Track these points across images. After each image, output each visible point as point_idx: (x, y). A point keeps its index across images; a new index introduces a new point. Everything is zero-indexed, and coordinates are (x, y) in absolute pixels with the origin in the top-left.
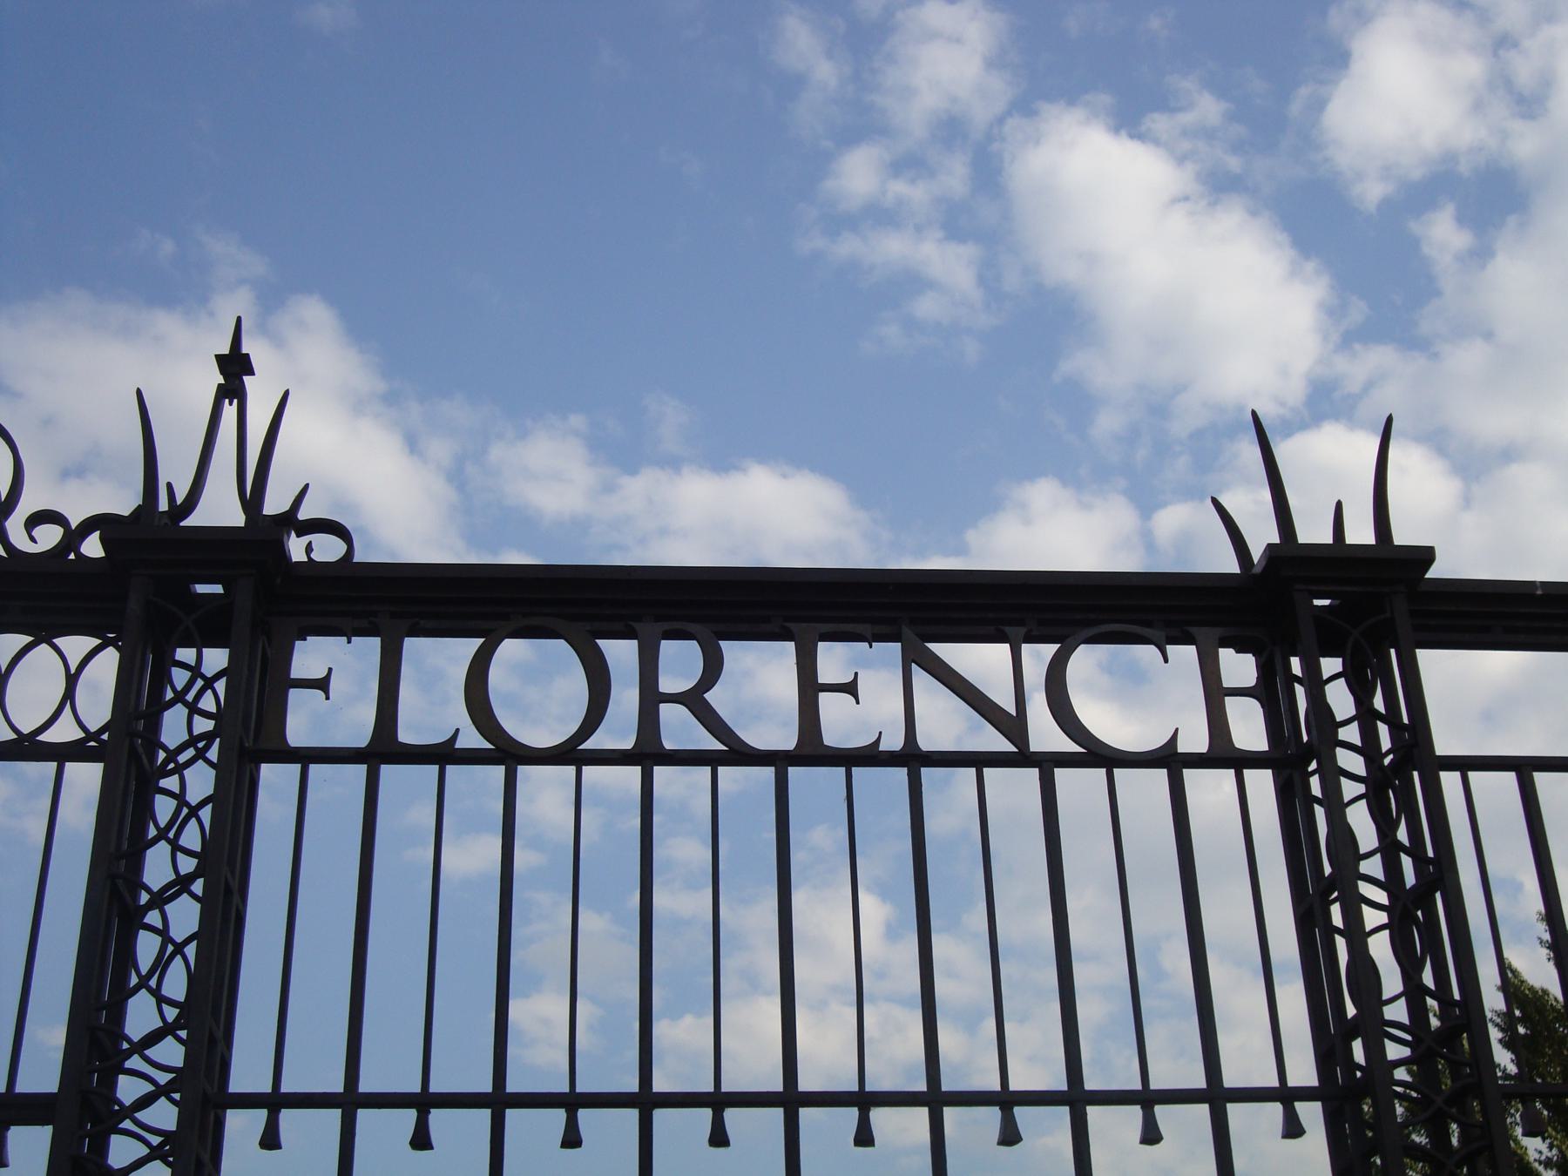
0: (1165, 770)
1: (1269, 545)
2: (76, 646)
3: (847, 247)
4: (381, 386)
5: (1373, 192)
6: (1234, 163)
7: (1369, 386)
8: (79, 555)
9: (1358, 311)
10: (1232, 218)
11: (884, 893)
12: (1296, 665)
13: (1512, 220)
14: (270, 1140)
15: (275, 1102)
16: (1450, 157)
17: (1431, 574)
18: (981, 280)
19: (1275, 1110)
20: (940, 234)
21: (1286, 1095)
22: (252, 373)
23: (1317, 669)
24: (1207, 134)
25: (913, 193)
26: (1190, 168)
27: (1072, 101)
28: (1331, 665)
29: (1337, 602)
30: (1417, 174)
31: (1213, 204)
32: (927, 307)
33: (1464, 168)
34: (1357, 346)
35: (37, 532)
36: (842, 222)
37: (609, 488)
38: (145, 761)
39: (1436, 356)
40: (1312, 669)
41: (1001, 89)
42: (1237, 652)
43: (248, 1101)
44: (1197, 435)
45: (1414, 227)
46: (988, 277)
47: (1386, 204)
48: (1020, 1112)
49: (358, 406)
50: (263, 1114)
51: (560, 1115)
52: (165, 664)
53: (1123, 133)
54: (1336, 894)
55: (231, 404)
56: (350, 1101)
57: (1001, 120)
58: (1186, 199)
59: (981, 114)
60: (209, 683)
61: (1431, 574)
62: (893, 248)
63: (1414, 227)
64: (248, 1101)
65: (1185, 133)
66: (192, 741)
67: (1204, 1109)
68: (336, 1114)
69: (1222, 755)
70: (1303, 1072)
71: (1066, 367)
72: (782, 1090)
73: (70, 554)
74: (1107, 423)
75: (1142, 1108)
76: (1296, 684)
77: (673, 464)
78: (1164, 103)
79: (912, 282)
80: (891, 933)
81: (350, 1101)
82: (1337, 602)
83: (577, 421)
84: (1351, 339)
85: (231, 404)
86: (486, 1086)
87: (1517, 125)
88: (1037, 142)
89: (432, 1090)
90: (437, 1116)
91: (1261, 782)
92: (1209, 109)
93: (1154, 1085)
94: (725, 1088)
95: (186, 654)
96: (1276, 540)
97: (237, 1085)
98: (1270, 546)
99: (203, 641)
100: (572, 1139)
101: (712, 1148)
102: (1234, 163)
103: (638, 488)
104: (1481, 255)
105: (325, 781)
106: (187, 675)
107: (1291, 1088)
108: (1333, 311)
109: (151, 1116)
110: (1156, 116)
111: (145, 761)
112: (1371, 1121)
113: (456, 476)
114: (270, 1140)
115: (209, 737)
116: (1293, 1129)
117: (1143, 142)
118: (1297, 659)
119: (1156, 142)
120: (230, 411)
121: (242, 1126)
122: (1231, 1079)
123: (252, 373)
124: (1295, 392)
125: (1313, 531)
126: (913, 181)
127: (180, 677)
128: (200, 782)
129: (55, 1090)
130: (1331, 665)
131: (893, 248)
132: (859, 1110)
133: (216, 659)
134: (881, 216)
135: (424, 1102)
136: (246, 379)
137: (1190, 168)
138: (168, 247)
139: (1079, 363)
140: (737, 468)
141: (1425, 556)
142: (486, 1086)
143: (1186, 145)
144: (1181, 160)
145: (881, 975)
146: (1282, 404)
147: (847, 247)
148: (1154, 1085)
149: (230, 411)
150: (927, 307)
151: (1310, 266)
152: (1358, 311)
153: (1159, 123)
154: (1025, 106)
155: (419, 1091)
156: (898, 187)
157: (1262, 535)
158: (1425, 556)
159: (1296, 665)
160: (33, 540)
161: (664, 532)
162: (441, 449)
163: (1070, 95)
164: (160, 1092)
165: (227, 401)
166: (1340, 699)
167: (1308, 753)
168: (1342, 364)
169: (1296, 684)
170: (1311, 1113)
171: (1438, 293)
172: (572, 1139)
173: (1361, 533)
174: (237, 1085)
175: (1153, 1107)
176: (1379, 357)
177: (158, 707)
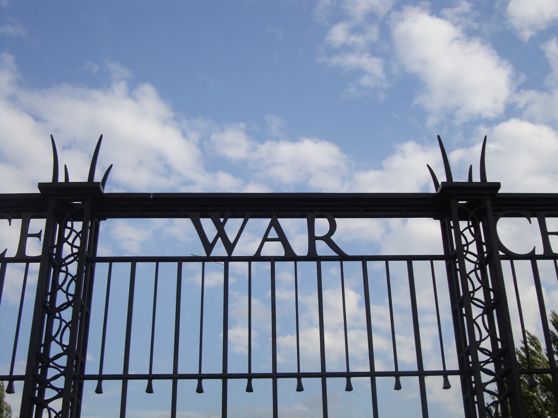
0: (406, 261)
3: (336, 60)
4: (173, 115)
5: (527, 35)
6: (475, 26)
7: (527, 106)
9: (523, 78)
10: (475, 45)
14: (99, 390)
15: (100, 378)
17: (500, 191)
18: (385, 71)
19: (441, 378)
20: (369, 54)
21: (445, 373)
24: (465, 15)
25: (359, 40)
26: (460, 28)
27: (415, 5)
28: (463, 225)
29: (468, 202)
30: (543, 28)
31: (468, 41)
32: (365, 81)
34: (522, 91)
36: (333, 51)
37: (254, 149)
39: (552, 94)
40: (457, 227)
42: (434, 219)
43: (19, 378)
44: (465, 124)
45: (542, 47)
46: (386, 68)
47: (531, 39)
49: (165, 122)
50: (96, 382)
51: (245, 381)
52: (63, 227)
53: (434, 16)
54: (492, 302)
56: (125, 377)
57: (389, 13)
58: (458, 39)
59: (382, 11)
61: (500, 191)
62: (352, 60)
63: (542, 47)
65: (457, 15)
67: (369, 379)
68: (171, 381)
70: (453, 364)
71: (416, 102)
74: (432, 121)
75: (443, 377)
77: (277, 139)
79: (359, 72)
81: (324, 375)
82: (468, 202)
83: (242, 125)
84: (520, 88)
86: (220, 371)
88: (403, 21)
93: (447, 369)
94: (301, 372)
97: (87, 372)
100: (200, 390)
101: (247, 392)
102: (475, 26)
103: (264, 149)
105: (100, 286)
106: (75, 244)
107: (376, 372)
108: (514, 78)
110: (445, 9)
113: (200, 146)
114: (99, 390)
116: (447, 386)
119: (447, 19)
121: (89, 386)
124: (500, 108)
125: (460, 177)
126: (358, 36)
129: (25, 374)
131: (352, 60)
132: (248, 379)
133: (78, 226)
134: (347, 49)
135: (150, 377)
137: (460, 28)
138: (96, 67)
139: (421, 100)
140: (299, 140)
141: (497, 186)
142: (171, 372)
143: (457, 19)
144: (456, 25)
146: (496, 113)
147: (336, 60)
150: (365, 81)
151: (505, 62)
152: (523, 78)
153: (447, 12)
156: (353, 38)
157: (442, 178)
158: (497, 186)
161: (274, 164)
162: (194, 136)
167: (455, 257)
168: (516, 98)
170: (455, 381)
171: (552, 71)
173: (477, 178)
174: (87, 372)
175: (301, 379)
176: (531, 95)
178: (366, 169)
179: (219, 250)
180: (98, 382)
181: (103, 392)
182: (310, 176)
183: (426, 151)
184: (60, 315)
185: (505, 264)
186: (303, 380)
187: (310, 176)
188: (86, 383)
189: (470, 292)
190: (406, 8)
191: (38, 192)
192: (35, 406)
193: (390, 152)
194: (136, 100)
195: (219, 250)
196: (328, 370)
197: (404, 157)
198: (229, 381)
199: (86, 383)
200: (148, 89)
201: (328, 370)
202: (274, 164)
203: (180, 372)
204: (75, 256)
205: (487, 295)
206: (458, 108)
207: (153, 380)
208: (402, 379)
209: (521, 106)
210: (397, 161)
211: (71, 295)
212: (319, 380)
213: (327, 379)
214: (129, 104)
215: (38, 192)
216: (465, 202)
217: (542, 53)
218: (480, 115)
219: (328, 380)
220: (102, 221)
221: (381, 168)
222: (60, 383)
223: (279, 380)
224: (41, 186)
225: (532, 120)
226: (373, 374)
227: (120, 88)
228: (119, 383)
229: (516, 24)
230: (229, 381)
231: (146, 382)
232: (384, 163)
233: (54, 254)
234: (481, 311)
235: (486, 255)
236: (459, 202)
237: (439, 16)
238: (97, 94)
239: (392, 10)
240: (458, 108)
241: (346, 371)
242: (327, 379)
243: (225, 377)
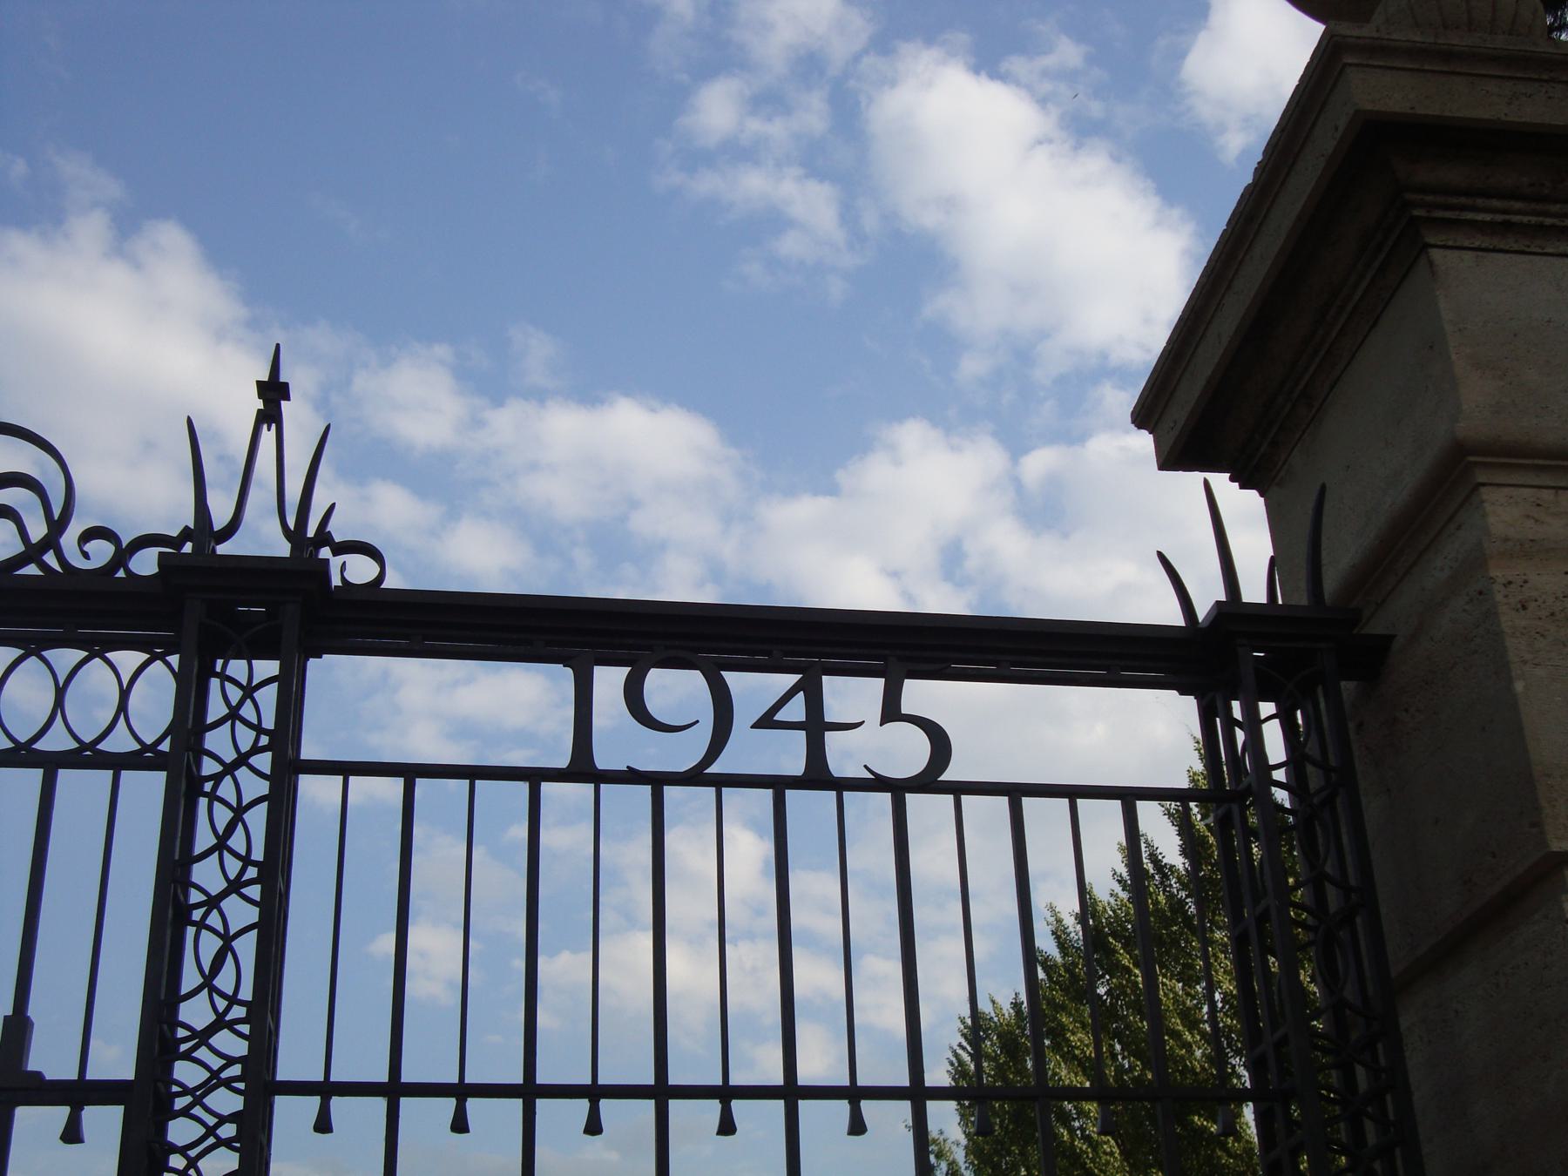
1: (1217, 601)
2: (127, 660)
3: (706, 184)
6: (1096, 109)
8: (128, 571)
10: (1095, 162)
12: (1236, 706)
15: (326, 1089)
19: (842, 1107)
22: (289, 399)
23: (1256, 711)
25: (777, 129)
27: (930, 40)
28: (1267, 708)
31: (1077, 147)
32: (790, 245)
35: (88, 547)
36: (698, 158)
37: (477, 423)
38: (195, 769)
41: (860, 27)
46: (848, 215)
48: (865, 1105)
49: (220, 334)
51: (583, 1105)
53: (983, 73)
55: (269, 430)
57: (857, 58)
58: (1050, 141)
59: (839, 51)
62: (754, 184)
65: (1046, 74)
72: (522, 1082)
73: (118, 570)
74: (972, 367)
76: (1237, 728)
77: (540, 396)
78: (1027, 46)
79: (773, 221)
81: (791, 1092)
83: (442, 351)
85: (269, 430)
86: (517, 1078)
88: (893, 83)
89: (333, 1079)
92: (1069, 53)
93: (861, 1082)
94: (601, 1081)
96: (1223, 599)
98: (1218, 602)
99: (253, 652)
102: (1096, 109)
103: (505, 422)
111: (195, 769)
112: (1300, 1118)
117: (1005, 83)
118: (1238, 702)
120: (268, 437)
121: (293, 1114)
122: (904, 1108)
123: (289, 399)
126: (769, 119)
131: (754, 184)
134: (739, 152)
136: (284, 404)
138: (20, 168)
140: (602, 402)
142: (383, 1077)
143: (1047, 86)
144: (1043, 102)
147: (706, 184)
148: (861, 1082)
149: (268, 437)
150: (790, 245)
151: (1176, 213)
153: (1017, 65)
154: (883, 44)
155: (590, 1083)
156: (755, 125)
157: (1207, 594)
159: (1236, 706)
160: (86, 555)
163: (930, 35)
165: (265, 426)
169: (1237, 728)
175: (859, 1102)
178: (791, 492)
180: (589, 1104)
181: (86, 1140)
182: (634, 504)
186: (737, 1105)
187: (634, 504)
189: (233, 812)
190: (906, 48)
193: (859, 446)
194: (137, 265)
197: (897, 462)
198: (541, 1104)
201: (673, 1080)
202: (534, 467)
206: (1044, 335)
207: (469, 1099)
210: (875, 473)
212: (779, 1105)
213: (403, 1100)
214: (117, 275)
218: (1104, 356)
219: (675, 1105)
220: (1195, 701)
221: (833, 490)
227: (90, 229)
228: (645, 1109)
230: (405, 1102)
231: (450, 1104)
232: (841, 476)
237: (996, 75)
239: (866, 51)
240: (1044, 335)
241: (588, 1081)
242: (403, 1100)
243: (661, 1092)
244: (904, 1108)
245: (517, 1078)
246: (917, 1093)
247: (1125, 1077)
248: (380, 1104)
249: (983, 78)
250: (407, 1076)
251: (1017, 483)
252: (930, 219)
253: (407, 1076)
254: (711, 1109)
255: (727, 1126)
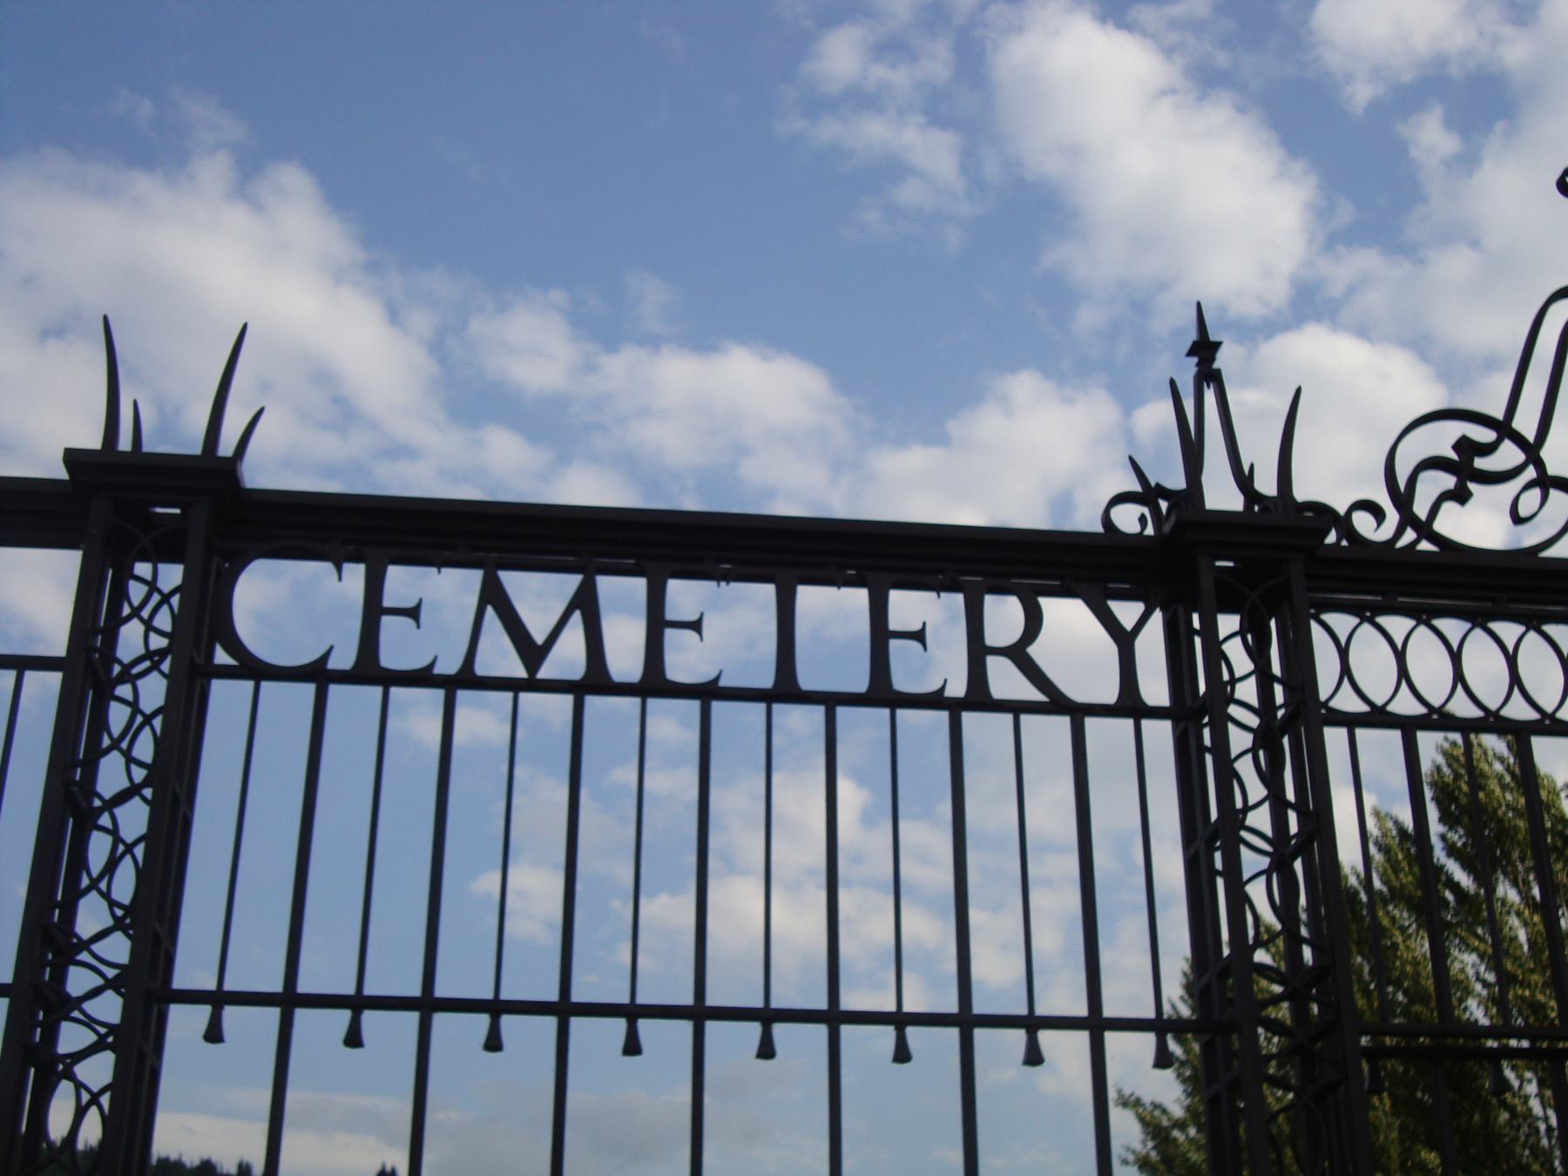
5: (1362, 94)
6: (1222, 59)
7: (1351, 290)
9: (1346, 213)
10: (1219, 113)
11: (860, 779)
13: (1499, 127)
14: (214, 1034)
15: (218, 999)
16: (1440, 61)
19: (1018, 1036)
24: (1194, 26)
25: (899, 77)
28: (1228, 623)
30: (1407, 77)
31: (1202, 98)
32: (909, 194)
33: (1453, 70)
34: (1341, 249)
36: (820, 105)
37: (590, 367)
39: (1421, 262)
40: (1209, 630)
43: (192, 997)
46: (969, 162)
47: (1375, 106)
48: (644, 1025)
49: (338, 276)
51: (484, 1020)
52: (124, 576)
56: (289, 1000)
58: (1173, 91)
60: (166, 599)
62: (875, 132)
64: (192, 997)
65: (1173, 24)
66: (148, 654)
69: (1130, 705)
74: (1088, 318)
77: (653, 342)
79: (893, 169)
80: (867, 819)
83: (558, 296)
86: (552, 995)
87: (1507, 31)
88: (1020, 30)
90: (370, 1018)
91: (1159, 734)
95: (143, 569)
97: (180, 981)
102: (1222, 59)
103: (619, 367)
104: (1468, 161)
108: (1320, 213)
109: (86, 1037)
113: (437, 349)
114: (214, 1034)
115: (162, 653)
121: (185, 1023)
122: (1082, 1038)
124: (1279, 293)
127: (137, 591)
128: (153, 691)
130: (1228, 623)
131: (875, 132)
133: (172, 575)
134: (862, 100)
135: (358, 1003)
138: (146, 108)
143: (1173, 37)
144: (1168, 52)
145: (857, 860)
147: (828, 130)
150: (909, 194)
151: (1298, 166)
152: (1346, 213)
153: (1146, 14)
156: (880, 72)
161: (645, 412)
162: (422, 321)
164: (110, 984)
166: (1238, 655)
167: (1288, 725)
172: (494, 1043)
174: (180, 981)
176: (1365, 260)
177: (116, 621)
178: (901, 442)
179: (500, 657)
182: (743, 450)
183: (1068, 401)
184: (114, 819)
185: (1335, 737)
186: (644, 1025)
187: (743, 450)
188: (177, 1013)
191: (62, 474)
192: (33, 1070)
193: (969, 396)
194: (258, 207)
195: (568, 658)
196: (979, 1007)
198: (710, 1026)
199: (177, 1013)
200: (294, 179)
202: (645, 412)
203: (303, 987)
204: (156, 658)
205: (1279, 821)
206: (1162, 286)
208: (780, 1030)
209: (1336, 290)
210: (986, 424)
211: (141, 764)
212: (821, 1031)
214: (237, 217)
215: (62, 474)
216: (1230, 564)
217: (1400, 148)
219: (980, 1034)
221: (942, 440)
222: (109, 1008)
223: (576, 1023)
224: (73, 458)
225: (1363, 332)
226: (834, 1017)
227: (214, 170)
228: (547, 1025)
229: (1333, 61)
230: (710, 1026)
231: (345, 1015)
232: (952, 426)
233: (96, 650)
234: (1265, 862)
235: (1280, 713)
236: (1218, 563)
237: (1124, 25)
238: (145, 184)
240: (1162, 286)
244: (1082, 1038)
245: (552, 995)
246: (1096, 1024)
247: (1396, 1021)
248: (413, 1018)
249: (1110, 27)
250: (712, 1000)
251: (1129, 435)
252: (1053, 167)
253: (712, 1000)
254: (885, 1036)
255: (632, 1047)
